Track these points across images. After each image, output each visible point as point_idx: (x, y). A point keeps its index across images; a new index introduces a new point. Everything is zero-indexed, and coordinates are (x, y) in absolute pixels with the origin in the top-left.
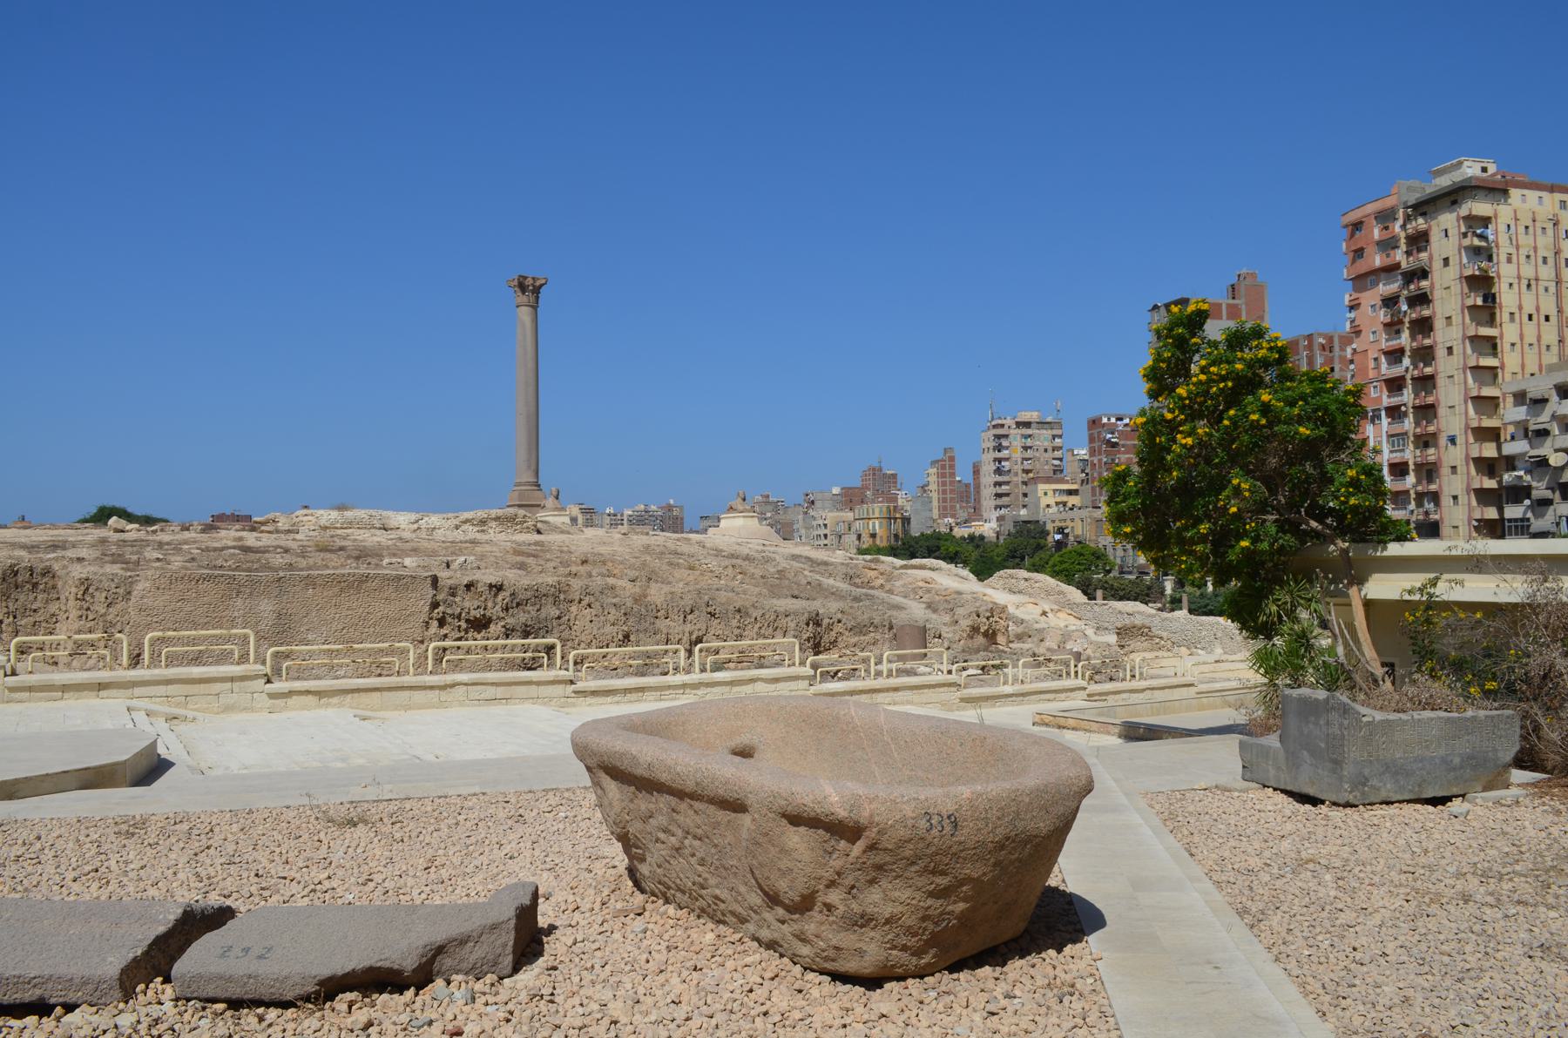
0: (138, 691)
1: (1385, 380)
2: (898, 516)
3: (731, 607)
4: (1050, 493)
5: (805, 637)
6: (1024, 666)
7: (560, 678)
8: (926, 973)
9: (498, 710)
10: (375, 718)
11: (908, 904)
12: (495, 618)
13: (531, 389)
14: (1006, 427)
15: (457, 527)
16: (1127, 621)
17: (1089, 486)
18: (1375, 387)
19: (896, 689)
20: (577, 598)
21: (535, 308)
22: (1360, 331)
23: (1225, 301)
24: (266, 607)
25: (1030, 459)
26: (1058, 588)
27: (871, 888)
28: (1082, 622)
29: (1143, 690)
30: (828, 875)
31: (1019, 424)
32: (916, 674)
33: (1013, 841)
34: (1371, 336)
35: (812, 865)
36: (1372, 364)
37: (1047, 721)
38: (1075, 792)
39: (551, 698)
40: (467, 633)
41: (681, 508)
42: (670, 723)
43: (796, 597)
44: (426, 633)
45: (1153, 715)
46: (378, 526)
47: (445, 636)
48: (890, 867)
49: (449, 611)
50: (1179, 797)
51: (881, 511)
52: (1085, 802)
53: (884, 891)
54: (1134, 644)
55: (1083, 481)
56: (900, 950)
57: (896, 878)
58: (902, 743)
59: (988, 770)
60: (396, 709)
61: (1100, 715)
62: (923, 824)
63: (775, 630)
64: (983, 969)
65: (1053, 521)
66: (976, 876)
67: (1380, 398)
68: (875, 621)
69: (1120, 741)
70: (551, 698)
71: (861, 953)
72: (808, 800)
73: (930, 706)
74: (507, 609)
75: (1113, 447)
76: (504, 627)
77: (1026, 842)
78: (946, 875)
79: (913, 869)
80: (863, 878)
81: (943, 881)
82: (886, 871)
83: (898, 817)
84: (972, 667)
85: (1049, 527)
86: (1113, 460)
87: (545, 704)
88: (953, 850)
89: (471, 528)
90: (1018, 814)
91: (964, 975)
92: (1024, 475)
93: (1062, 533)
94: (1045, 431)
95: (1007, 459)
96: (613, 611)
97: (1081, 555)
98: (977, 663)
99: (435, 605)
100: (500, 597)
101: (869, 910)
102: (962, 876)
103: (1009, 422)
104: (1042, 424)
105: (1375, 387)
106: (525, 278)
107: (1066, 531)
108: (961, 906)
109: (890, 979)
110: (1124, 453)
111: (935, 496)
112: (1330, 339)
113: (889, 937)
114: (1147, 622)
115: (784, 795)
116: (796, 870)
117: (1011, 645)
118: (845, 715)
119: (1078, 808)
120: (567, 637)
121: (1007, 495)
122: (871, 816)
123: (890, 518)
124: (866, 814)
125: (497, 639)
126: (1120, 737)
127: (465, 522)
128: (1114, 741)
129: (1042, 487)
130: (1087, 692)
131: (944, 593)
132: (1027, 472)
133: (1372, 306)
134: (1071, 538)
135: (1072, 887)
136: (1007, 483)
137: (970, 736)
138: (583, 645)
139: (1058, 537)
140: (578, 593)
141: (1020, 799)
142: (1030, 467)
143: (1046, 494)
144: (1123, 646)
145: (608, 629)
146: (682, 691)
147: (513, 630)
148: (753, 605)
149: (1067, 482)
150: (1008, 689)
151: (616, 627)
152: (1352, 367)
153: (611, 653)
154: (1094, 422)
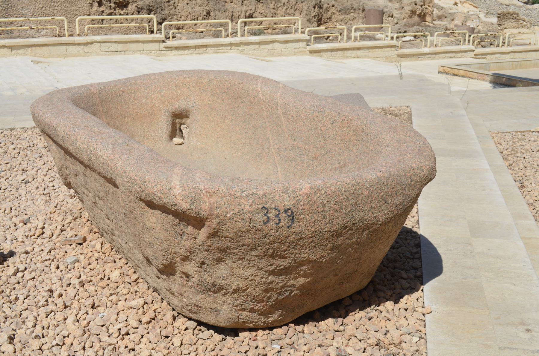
5: (313, 15)
6: (438, 35)
7: (156, 39)
8: (274, 325)
9: (119, 58)
10: (44, 62)
11: (252, 280)
16: (505, 10)
19: (359, 49)
27: (219, 265)
28: (479, 9)
29: (509, 53)
30: (182, 252)
32: (375, 39)
33: (351, 229)
35: (168, 243)
37: (447, 71)
38: (416, 182)
39: (151, 51)
40: (115, 10)
42: (123, 92)
44: (91, 10)
45: (512, 69)
47: (103, 12)
48: (233, 251)
50: (520, 136)
52: (425, 189)
53: (230, 269)
54: (507, 24)
56: (249, 312)
57: (240, 259)
58: (290, 117)
59: (351, 148)
60: (58, 57)
61: (480, 68)
62: (260, 217)
63: (295, 10)
64: (326, 321)
66: (314, 259)
68: (354, 6)
69: (491, 85)
70: (151, 51)
71: (216, 311)
72: (156, 190)
73: (379, 59)
76: (136, 6)
77: (367, 227)
78: (286, 258)
79: (254, 253)
80: (210, 258)
81: (283, 263)
82: (230, 254)
83: (236, 210)
84: (409, 36)
87: (148, 54)
88: (292, 238)
90: (356, 205)
91: (309, 327)
98: (411, 34)
101: (218, 282)
102: (300, 259)
108: (301, 281)
109: (244, 330)
113: (238, 302)
114: (516, 11)
115: (139, 182)
116: (155, 245)
117: (434, 22)
118: (253, 90)
119: (418, 195)
120: (173, 13)
122: (211, 209)
124: (206, 207)
125: (132, 14)
126: (490, 83)
128: (486, 85)
130: (475, 53)
135: (423, 231)
137: (340, 117)
138: (183, 18)
141: (360, 192)
144: (500, 25)
145: (198, 8)
146: (229, 48)
147: (142, 9)
150: (427, 50)
151: (202, 8)
153: (199, 23)
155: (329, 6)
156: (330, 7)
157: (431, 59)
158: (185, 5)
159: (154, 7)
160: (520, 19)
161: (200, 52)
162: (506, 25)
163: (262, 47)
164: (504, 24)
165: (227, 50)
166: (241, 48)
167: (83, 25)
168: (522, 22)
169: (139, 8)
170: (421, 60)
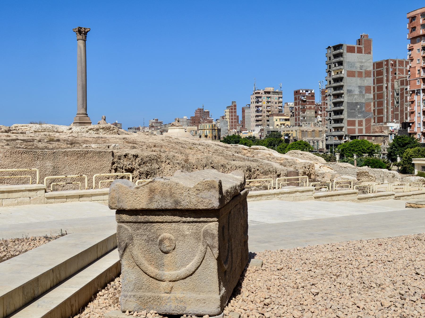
0: (93, 198)
1: (422, 79)
2: (216, 128)
3: (220, 164)
4: (278, 120)
12: (136, 168)
13: (84, 75)
14: (261, 93)
15: (87, 132)
17: (294, 117)
18: (418, 81)
20: (164, 160)
21: (85, 41)
22: (413, 59)
23: (356, 46)
24: (49, 164)
25: (270, 106)
26: (314, 158)
31: (266, 92)
34: (417, 61)
36: (417, 72)
37: (413, 206)
41: (121, 124)
43: (234, 160)
46: (56, 131)
49: (119, 166)
51: (209, 126)
55: (291, 115)
65: (284, 131)
67: (420, 85)
68: (271, 170)
74: (140, 165)
75: (304, 102)
76: (139, 172)
85: (282, 133)
86: (304, 107)
89: (93, 132)
92: (267, 113)
93: (288, 136)
94: (276, 95)
95: (261, 106)
96: (178, 166)
97: (300, 144)
99: (113, 163)
100: (137, 160)
103: (261, 91)
104: (275, 93)
105: (418, 81)
106: (81, 28)
107: (289, 135)
110: (308, 104)
111: (228, 120)
112: (395, 62)
121: (261, 120)
123: (213, 129)
127: (90, 129)
129: (275, 118)
130: (395, 196)
131: (280, 159)
132: (268, 111)
133: (418, 50)
134: (291, 138)
136: (261, 116)
139: (286, 137)
140: (164, 158)
142: (269, 110)
143: (277, 120)
144: (359, 180)
147: (142, 174)
148: (227, 164)
149: (285, 116)
152: (409, 73)
154: (297, 92)
155: (255, 170)
156: (255, 170)
157: (374, 200)
158: (168, 171)
159: (150, 172)
160: (370, 176)
161: (258, 199)
162: (362, 180)
163: (291, 195)
164: (361, 179)
165: (272, 198)
166: (280, 196)
167: (104, 185)
168: (371, 177)
169: (140, 173)
170: (369, 201)
